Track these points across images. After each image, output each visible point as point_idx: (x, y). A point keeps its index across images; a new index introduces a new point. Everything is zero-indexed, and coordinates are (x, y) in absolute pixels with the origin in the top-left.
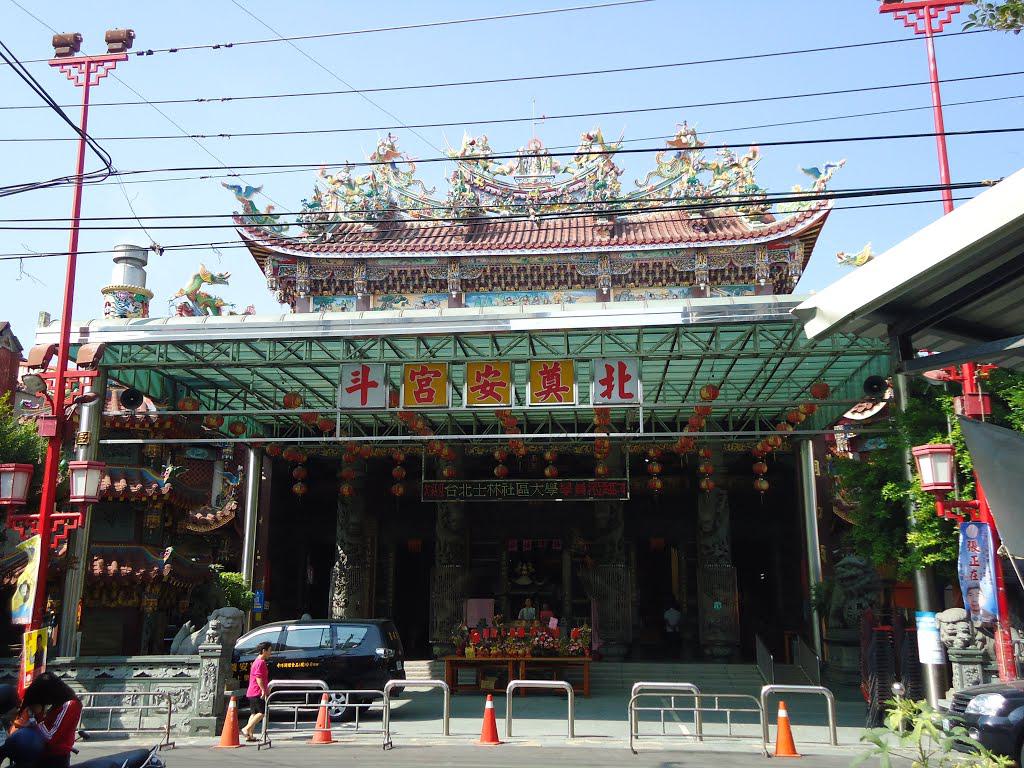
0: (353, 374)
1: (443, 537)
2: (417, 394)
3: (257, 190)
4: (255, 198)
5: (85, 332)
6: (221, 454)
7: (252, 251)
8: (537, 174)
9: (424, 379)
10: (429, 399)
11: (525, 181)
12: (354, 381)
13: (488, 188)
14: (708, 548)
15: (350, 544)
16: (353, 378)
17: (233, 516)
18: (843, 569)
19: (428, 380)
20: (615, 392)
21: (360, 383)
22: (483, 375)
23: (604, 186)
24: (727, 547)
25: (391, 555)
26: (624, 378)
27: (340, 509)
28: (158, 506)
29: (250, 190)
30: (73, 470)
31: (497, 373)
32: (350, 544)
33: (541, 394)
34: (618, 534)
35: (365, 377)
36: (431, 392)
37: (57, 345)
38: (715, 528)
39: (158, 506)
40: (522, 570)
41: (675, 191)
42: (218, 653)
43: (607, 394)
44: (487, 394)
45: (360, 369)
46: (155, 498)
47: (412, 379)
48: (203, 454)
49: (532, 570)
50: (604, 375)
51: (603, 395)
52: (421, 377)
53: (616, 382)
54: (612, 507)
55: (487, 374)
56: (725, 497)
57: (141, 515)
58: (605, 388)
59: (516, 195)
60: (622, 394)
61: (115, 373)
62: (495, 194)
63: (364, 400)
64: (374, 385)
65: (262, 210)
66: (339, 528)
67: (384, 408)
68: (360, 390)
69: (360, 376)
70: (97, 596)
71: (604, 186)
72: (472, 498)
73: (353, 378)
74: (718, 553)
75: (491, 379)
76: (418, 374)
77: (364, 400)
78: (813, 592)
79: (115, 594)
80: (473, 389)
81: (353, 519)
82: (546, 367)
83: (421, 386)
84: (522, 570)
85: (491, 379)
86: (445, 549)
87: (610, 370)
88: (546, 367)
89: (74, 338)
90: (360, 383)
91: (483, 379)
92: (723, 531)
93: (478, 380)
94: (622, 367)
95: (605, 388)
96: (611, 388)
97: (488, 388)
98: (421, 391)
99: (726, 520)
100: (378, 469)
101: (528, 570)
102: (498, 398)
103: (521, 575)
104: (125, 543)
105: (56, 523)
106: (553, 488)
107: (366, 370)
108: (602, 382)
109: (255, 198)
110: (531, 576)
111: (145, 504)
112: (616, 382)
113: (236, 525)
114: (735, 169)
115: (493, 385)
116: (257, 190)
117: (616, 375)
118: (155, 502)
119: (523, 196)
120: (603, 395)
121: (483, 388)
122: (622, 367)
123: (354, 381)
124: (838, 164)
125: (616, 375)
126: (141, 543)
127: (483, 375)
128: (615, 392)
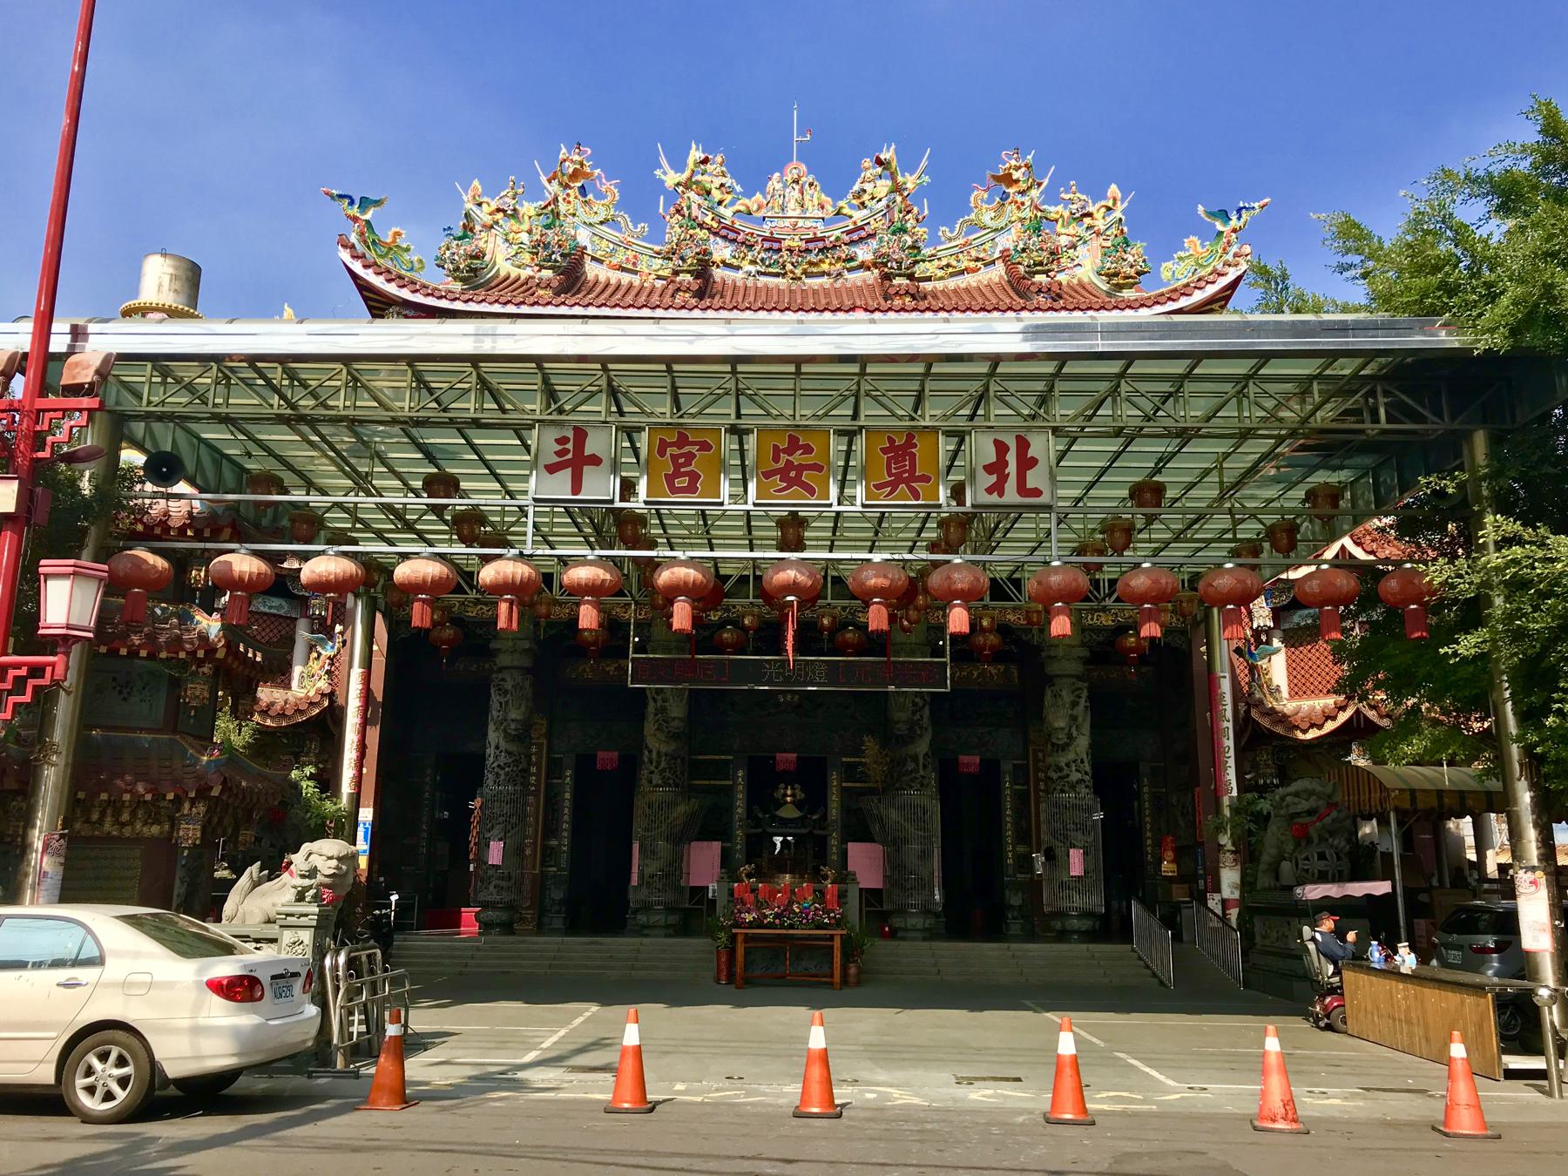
0: (558, 441)
1: (656, 742)
2: (670, 479)
5: (77, 333)
6: (308, 608)
7: (366, 299)
8: (795, 214)
9: (681, 456)
10: (691, 489)
11: (781, 223)
13: (724, 232)
14: (1060, 769)
15: (509, 753)
17: (326, 704)
18: (1296, 800)
19: (690, 457)
20: (1011, 485)
21: (570, 456)
22: (784, 451)
23: (903, 230)
24: (1088, 768)
25: (568, 773)
26: (1026, 463)
27: (495, 699)
28: (205, 670)
31: (808, 450)
32: (509, 753)
33: (878, 487)
34: (922, 747)
36: (694, 477)
37: (25, 356)
39: (205, 670)
40: (785, 795)
41: (1000, 248)
42: (312, 921)
43: (998, 488)
44: (797, 481)
45: (570, 434)
46: (201, 654)
47: (662, 453)
48: (281, 607)
49: (800, 795)
50: (991, 457)
51: (990, 491)
52: (675, 451)
56: (1085, 694)
57: (176, 684)
58: (993, 479)
60: (1022, 489)
61: (139, 428)
63: (576, 487)
64: (595, 460)
66: (491, 727)
67: (612, 502)
68: (569, 470)
69: (570, 446)
70: (95, 817)
71: (903, 230)
72: (538, 765)
74: (1075, 776)
75: (797, 458)
76: (672, 445)
77: (576, 487)
78: (1225, 840)
80: (767, 475)
81: (514, 714)
82: (891, 440)
83: (677, 466)
84: (785, 795)
85: (797, 458)
86: (659, 763)
87: (1001, 448)
88: (891, 440)
90: (570, 456)
91: (784, 457)
92: (1083, 743)
93: (776, 459)
95: (993, 479)
96: (1003, 478)
98: (678, 473)
101: (793, 795)
102: (812, 491)
104: (149, 731)
105: (12, 673)
107: (580, 435)
108: (989, 469)
110: (798, 804)
111: (184, 665)
113: (328, 721)
114: (1087, 221)
115: (801, 468)
117: (1011, 457)
118: (200, 663)
119: (776, 246)
120: (990, 491)
121: (783, 474)
122: (1023, 445)
123: (558, 454)
124: (1256, 205)
125: (1011, 457)
126: (175, 731)
127: (784, 451)
128: (1011, 485)
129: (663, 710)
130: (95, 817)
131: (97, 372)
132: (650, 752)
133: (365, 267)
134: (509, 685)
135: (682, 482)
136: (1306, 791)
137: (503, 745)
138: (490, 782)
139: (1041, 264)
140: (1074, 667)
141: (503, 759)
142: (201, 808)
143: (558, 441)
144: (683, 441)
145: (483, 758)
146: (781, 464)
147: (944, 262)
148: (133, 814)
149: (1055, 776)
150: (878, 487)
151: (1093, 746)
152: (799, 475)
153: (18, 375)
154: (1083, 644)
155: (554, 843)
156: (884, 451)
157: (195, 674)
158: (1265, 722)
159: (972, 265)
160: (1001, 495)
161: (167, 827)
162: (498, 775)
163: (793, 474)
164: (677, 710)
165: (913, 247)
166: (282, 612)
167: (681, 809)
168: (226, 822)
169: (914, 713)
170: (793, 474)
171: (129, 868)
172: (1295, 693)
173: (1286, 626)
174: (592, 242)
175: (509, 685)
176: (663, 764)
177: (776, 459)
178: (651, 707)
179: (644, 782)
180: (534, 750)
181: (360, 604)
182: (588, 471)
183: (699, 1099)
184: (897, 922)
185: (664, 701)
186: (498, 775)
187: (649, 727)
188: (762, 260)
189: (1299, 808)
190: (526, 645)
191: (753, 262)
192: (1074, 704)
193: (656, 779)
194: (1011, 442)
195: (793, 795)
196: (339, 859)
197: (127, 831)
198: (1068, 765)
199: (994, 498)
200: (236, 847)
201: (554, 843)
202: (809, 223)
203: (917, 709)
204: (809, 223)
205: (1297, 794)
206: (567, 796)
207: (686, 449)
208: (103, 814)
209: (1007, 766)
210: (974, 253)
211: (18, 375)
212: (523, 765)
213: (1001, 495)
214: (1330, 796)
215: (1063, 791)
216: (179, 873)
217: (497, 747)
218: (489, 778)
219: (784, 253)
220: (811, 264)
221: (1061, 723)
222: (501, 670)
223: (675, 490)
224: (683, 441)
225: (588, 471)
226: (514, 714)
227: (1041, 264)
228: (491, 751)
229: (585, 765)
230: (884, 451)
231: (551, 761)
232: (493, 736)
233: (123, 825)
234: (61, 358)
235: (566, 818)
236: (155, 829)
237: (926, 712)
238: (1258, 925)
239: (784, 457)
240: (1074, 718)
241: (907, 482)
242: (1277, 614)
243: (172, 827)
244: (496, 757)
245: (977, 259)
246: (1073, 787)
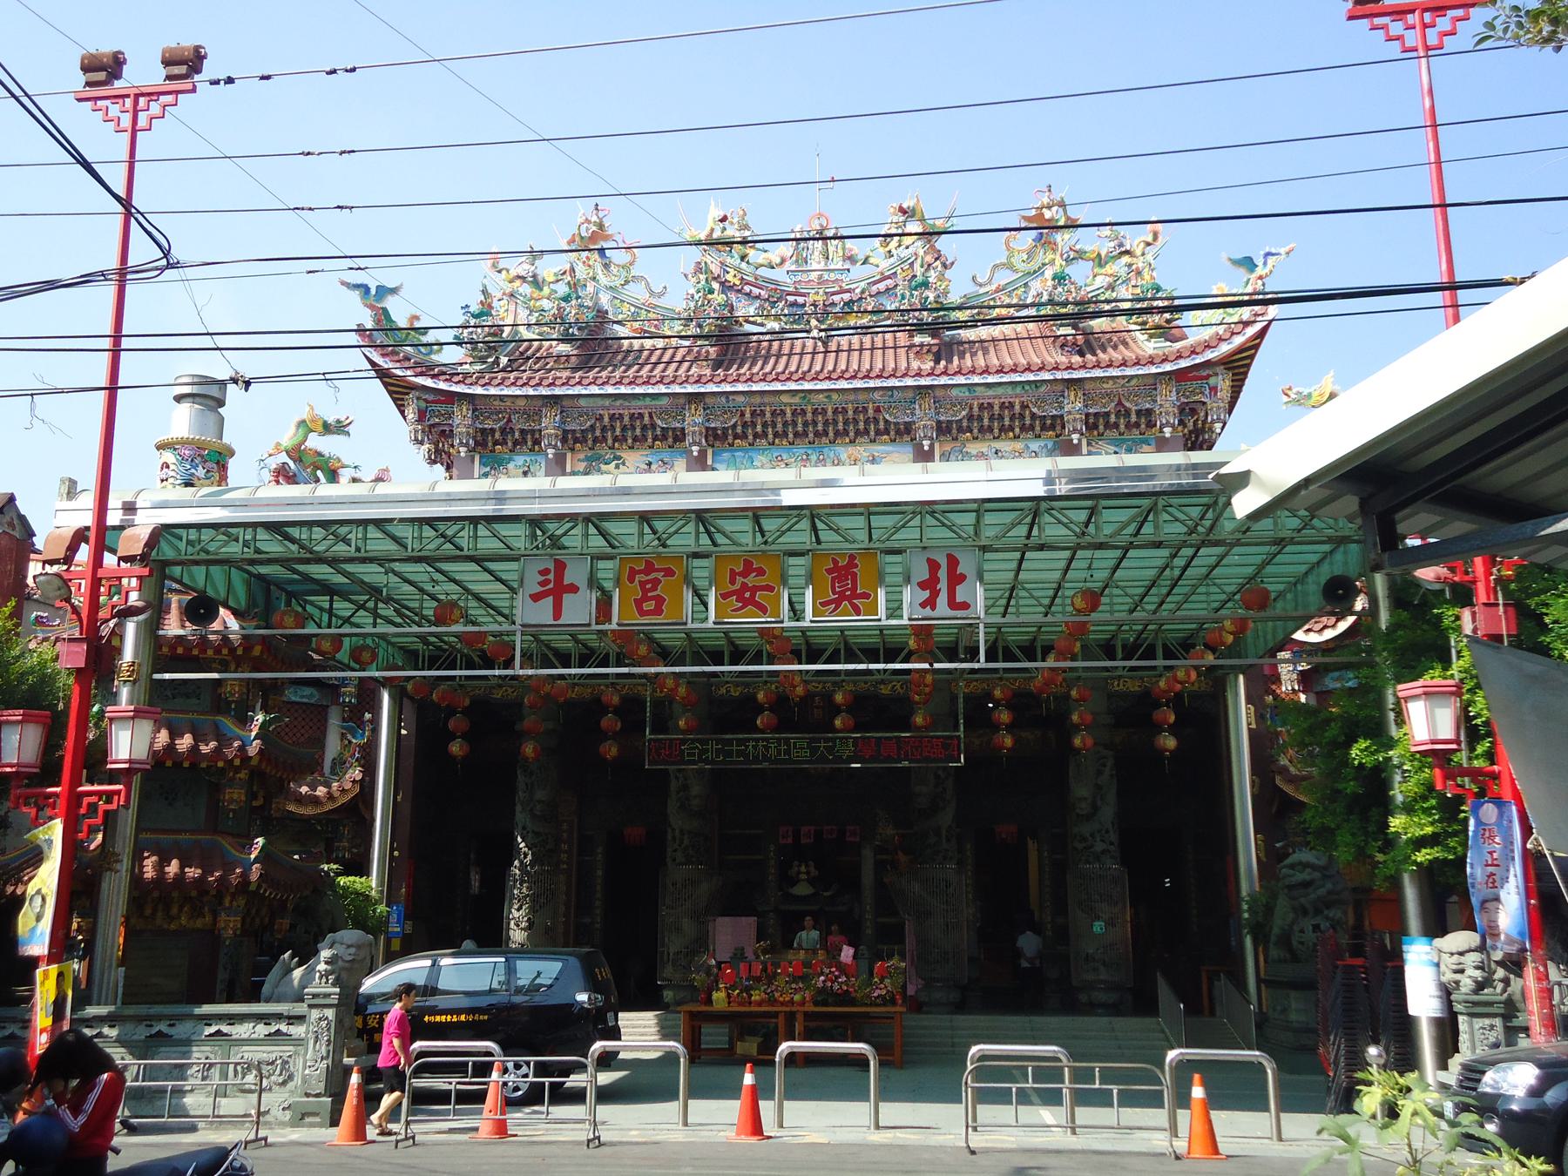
2: (639, 603)
4: (391, 303)
5: (130, 508)
6: (339, 695)
7: (386, 385)
8: (822, 266)
9: (648, 582)
10: (658, 611)
11: (804, 277)
13: (747, 289)
14: (1084, 839)
19: (656, 582)
20: (942, 600)
24: (1113, 837)
25: (600, 850)
26: (956, 579)
29: (383, 291)
30: (111, 719)
31: (761, 572)
33: (824, 604)
34: (946, 818)
36: (660, 600)
37: (87, 528)
38: (1095, 808)
40: (799, 873)
42: (334, 1000)
44: (752, 601)
47: (631, 580)
49: (814, 872)
51: (923, 605)
53: (943, 585)
55: (745, 574)
56: (1110, 763)
57: (216, 789)
58: (926, 594)
59: (791, 298)
60: (953, 604)
62: (758, 297)
64: (573, 589)
66: (518, 808)
69: (551, 576)
70: (148, 912)
71: (925, 285)
74: (1099, 846)
75: (751, 580)
76: (640, 572)
77: (557, 613)
80: (725, 596)
82: (835, 562)
83: (645, 591)
84: (799, 873)
85: (751, 580)
87: (933, 566)
88: (835, 562)
89: (113, 518)
91: (739, 580)
92: (1108, 813)
93: (733, 582)
95: (926, 594)
98: (645, 598)
100: (579, 717)
101: (808, 873)
102: (764, 610)
105: (86, 800)
109: (391, 303)
112: (943, 585)
114: (1126, 259)
115: (755, 589)
116: (394, 291)
117: (943, 574)
118: (237, 770)
120: (923, 605)
121: (739, 594)
123: (542, 584)
125: (943, 574)
126: (215, 831)
127: (740, 574)
128: (942, 600)
129: (685, 788)
130: (148, 912)
131: (146, 545)
135: (649, 606)
136: (1300, 863)
143: (542, 573)
144: (649, 568)
146: (737, 586)
148: (155, 911)
149: (1080, 846)
150: (824, 604)
152: (753, 596)
153: (83, 545)
155: (587, 920)
156: (829, 571)
157: (234, 778)
160: (933, 608)
163: (747, 595)
170: (747, 595)
174: (614, 306)
176: (686, 842)
177: (733, 582)
178: (674, 785)
179: (669, 860)
180: (565, 827)
182: (567, 598)
187: (672, 806)
189: (1293, 880)
192: (1100, 773)
195: (808, 873)
196: (359, 947)
198: (1092, 835)
201: (587, 920)
202: (833, 276)
204: (833, 276)
205: (1292, 866)
206: (600, 873)
207: (653, 576)
208: (155, 911)
211: (83, 545)
213: (933, 608)
214: (1325, 868)
223: (642, 613)
224: (649, 568)
225: (567, 598)
226: (540, 794)
230: (829, 571)
235: (598, 895)
239: (739, 580)
240: (1098, 787)
241: (850, 599)
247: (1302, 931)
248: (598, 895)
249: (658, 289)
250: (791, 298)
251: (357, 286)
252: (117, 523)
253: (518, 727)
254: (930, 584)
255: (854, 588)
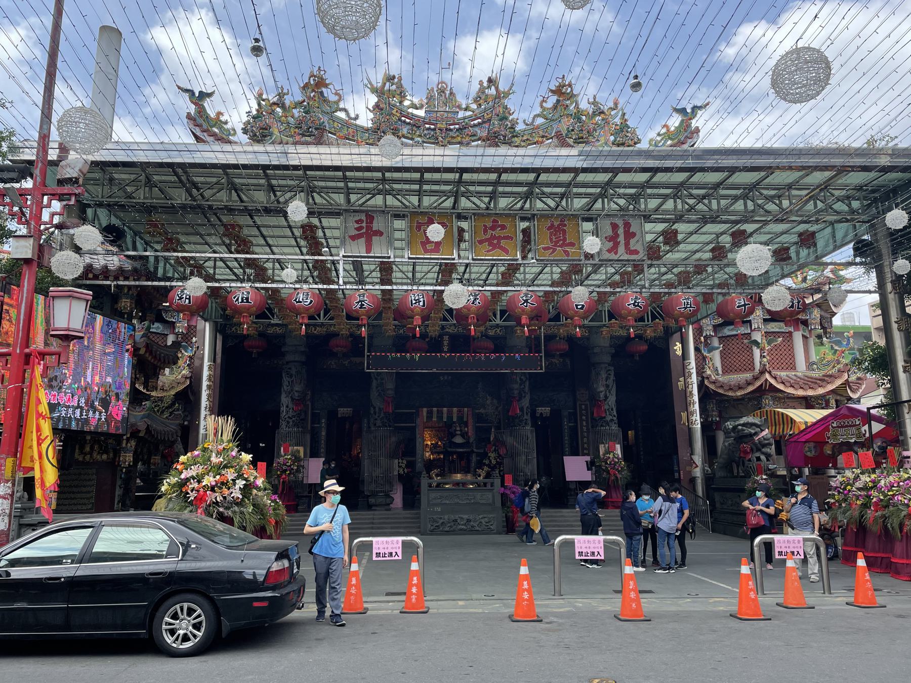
0: (357, 222)
3: (210, 95)
4: (207, 104)
5: (64, 149)
6: (174, 328)
12: (358, 229)
16: (357, 226)
17: (188, 383)
20: (621, 249)
21: (364, 230)
26: (629, 235)
27: (286, 380)
29: (203, 95)
30: (53, 297)
31: (503, 227)
35: (369, 228)
38: (606, 397)
40: (456, 430)
44: (494, 247)
45: (364, 218)
48: (158, 328)
51: (609, 251)
53: (621, 239)
54: (521, 379)
55: (493, 228)
56: (612, 373)
58: (611, 244)
59: (427, 126)
62: (409, 124)
64: (379, 233)
65: (212, 115)
66: (283, 396)
69: (364, 225)
70: (88, 449)
73: (357, 226)
74: (609, 418)
75: (498, 232)
79: (88, 449)
84: (456, 430)
87: (615, 227)
89: (53, 155)
92: (612, 399)
93: (485, 231)
94: (627, 225)
95: (611, 244)
97: (495, 242)
99: (614, 391)
100: (319, 346)
102: (506, 251)
103: (456, 435)
106: (480, 361)
109: (207, 104)
112: (621, 239)
114: (602, 115)
116: (210, 95)
117: (621, 231)
120: (609, 251)
122: (627, 225)
123: (358, 229)
125: (621, 231)
128: (621, 249)
132: (374, 408)
133: (203, 131)
134: (293, 371)
137: (291, 406)
138: (284, 426)
139: (582, 138)
140: (607, 359)
141: (291, 414)
142: (133, 443)
143: (357, 222)
145: (278, 413)
146: (488, 236)
147: (525, 138)
148: (92, 448)
151: (618, 402)
152: (499, 243)
154: (611, 346)
158: (712, 387)
159: (540, 139)
160: (616, 253)
161: (111, 455)
162: (288, 422)
164: (390, 385)
165: (512, 128)
166: (159, 331)
167: (393, 439)
168: (145, 450)
169: (521, 385)
171: (89, 480)
172: (725, 371)
173: (720, 335)
175: (293, 371)
177: (485, 231)
178: (374, 383)
181: (207, 325)
182: (375, 239)
183: (480, 611)
184: (372, 501)
185: (382, 379)
186: (288, 422)
187: (374, 394)
188: (425, 135)
190: (303, 349)
191: (420, 136)
193: (379, 423)
194: (620, 223)
197: (88, 457)
199: (612, 256)
200: (149, 466)
203: (522, 382)
205: (743, 425)
209: (565, 413)
210: (541, 133)
212: (303, 417)
213: (616, 253)
215: (602, 426)
216: (119, 482)
217: (287, 407)
218: (283, 424)
219: (438, 131)
220: (453, 137)
221: (602, 389)
222: (287, 363)
225: (375, 239)
226: (297, 388)
227: (582, 138)
228: (283, 409)
229: (332, 415)
231: (313, 414)
232: (285, 400)
233: (86, 454)
234: (55, 164)
236: (105, 457)
237: (527, 383)
238: (717, 497)
242: (716, 328)
243: (115, 456)
244: (287, 412)
245: (543, 137)
246: (608, 424)
247: (750, 460)
248: (323, 446)
249: (353, 116)
250: (427, 126)
251: (187, 91)
252: (55, 158)
253: (283, 350)
254: (613, 238)
255: (565, 239)
